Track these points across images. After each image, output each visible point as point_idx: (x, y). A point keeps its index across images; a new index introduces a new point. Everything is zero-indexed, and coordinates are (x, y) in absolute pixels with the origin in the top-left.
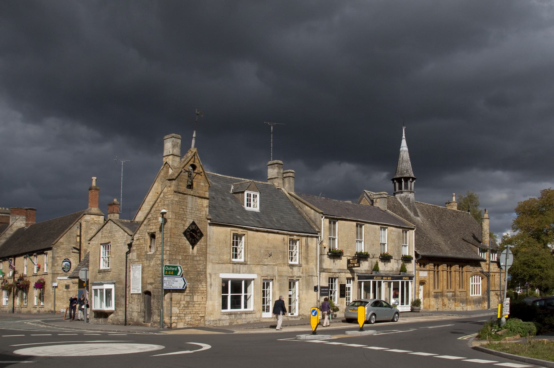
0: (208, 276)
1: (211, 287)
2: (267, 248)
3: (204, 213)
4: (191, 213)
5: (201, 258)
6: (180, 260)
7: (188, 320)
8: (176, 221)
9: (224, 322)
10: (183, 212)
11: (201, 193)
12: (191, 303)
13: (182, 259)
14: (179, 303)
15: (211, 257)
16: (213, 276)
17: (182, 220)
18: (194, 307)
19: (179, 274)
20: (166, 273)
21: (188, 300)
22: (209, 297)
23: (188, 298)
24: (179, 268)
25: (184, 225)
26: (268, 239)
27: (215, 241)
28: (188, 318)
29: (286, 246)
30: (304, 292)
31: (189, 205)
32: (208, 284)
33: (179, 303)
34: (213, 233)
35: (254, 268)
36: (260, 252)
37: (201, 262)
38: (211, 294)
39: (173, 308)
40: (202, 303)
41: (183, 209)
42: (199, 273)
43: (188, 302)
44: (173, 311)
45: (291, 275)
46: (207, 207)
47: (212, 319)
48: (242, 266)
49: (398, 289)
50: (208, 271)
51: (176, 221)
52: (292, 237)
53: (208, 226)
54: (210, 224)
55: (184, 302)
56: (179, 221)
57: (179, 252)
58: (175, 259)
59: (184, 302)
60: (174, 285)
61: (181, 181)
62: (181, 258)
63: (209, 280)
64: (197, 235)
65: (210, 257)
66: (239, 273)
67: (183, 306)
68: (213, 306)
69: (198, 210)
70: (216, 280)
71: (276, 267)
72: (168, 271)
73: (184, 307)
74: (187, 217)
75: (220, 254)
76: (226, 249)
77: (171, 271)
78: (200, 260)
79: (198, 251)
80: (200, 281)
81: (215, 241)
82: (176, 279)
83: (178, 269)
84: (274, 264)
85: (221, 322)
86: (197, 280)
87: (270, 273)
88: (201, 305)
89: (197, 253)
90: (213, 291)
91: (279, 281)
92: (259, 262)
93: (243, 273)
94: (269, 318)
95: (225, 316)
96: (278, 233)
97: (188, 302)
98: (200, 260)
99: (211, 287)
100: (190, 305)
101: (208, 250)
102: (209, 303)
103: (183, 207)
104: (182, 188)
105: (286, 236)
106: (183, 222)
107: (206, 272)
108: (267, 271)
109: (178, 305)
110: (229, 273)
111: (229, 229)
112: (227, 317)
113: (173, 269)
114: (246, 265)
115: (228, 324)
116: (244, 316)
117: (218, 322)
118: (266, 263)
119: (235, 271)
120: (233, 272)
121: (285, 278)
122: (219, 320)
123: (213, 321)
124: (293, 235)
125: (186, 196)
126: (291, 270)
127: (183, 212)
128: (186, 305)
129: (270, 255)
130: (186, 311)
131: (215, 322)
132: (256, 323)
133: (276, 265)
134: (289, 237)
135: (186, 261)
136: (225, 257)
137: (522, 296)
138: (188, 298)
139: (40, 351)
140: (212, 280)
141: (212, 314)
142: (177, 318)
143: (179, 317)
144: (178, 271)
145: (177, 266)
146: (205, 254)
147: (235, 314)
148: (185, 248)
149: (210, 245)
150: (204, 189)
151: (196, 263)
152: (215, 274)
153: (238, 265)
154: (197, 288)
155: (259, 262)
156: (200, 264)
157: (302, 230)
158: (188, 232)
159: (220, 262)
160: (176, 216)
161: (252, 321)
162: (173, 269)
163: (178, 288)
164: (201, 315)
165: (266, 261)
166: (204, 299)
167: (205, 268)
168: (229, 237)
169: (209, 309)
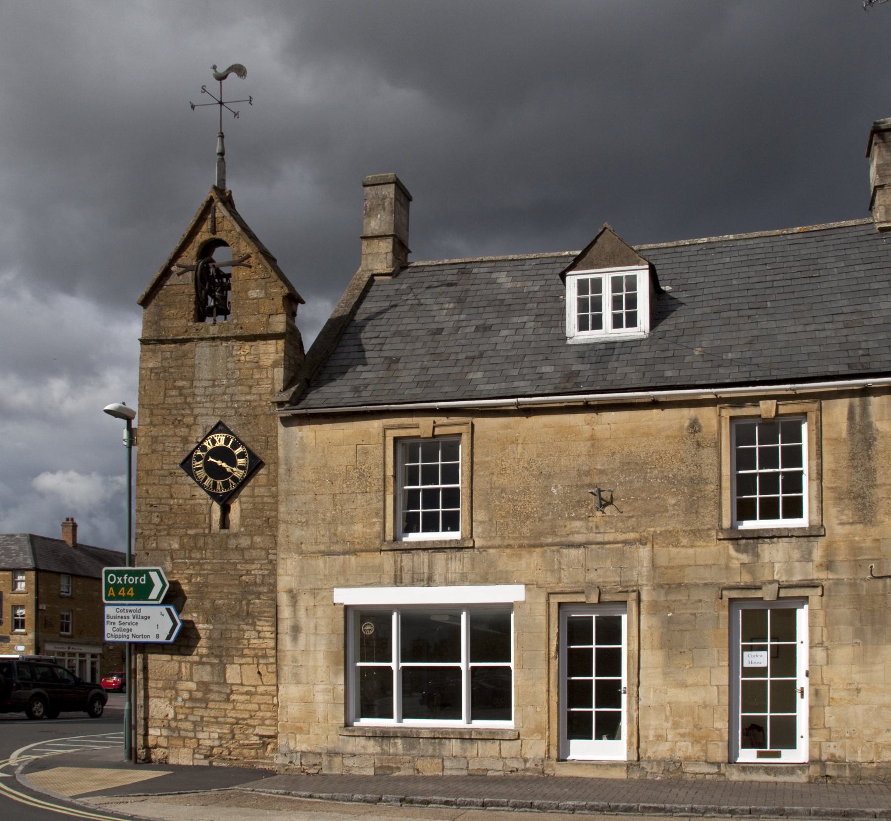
0: (283, 599)
1: (295, 639)
2: (580, 474)
3: (266, 387)
4: (211, 397)
5: (258, 539)
6: (172, 552)
7: (208, 743)
8: (155, 431)
9: (349, 762)
10: (179, 400)
11: (252, 323)
12: (214, 688)
13: (182, 547)
14: (172, 685)
15: (297, 533)
16: (305, 601)
17: (177, 423)
18: (228, 700)
19: (154, 594)
20: (112, 592)
21: (206, 678)
22: (286, 670)
23: (204, 674)
24: (154, 576)
25: (185, 440)
26: (593, 438)
27: (311, 476)
28: (209, 737)
29: (708, 454)
30: (843, 654)
31: (204, 373)
32: (285, 626)
33: (173, 688)
34: (303, 448)
35: (505, 561)
36: (546, 491)
37: (255, 553)
38: (295, 660)
39: (153, 702)
40: (261, 689)
41: (181, 388)
42: (247, 590)
43: (204, 686)
44: (153, 712)
45: (746, 579)
46: (275, 365)
47: (304, 747)
48: (440, 557)
49: (751, 646)
50: (285, 581)
51: (155, 431)
52: (748, 411)
53: (281, 429)
54: (287, 422)
55: (192, 686)
56: (168, 430)
57: (170, 527)
58: (157, 549)
59: (192, 686)
60: (136, 630)
61: (170, 305)
62: (176, 546)
63: (285, 612)
64: (233, 463)
65: (290, 533)
66: (429, 581)
67: (186, 695)
68: (306, 701)
69: (239, 382)
70: (320, 612)
71: (644, 552)
72: (117, 587)
73: (191, 699)
74: (197, 411)
75: (334, 521)
76: (360, 499)
77: (127, 586)
78: (252, 547)
79: (243, 517)
80: (250, 617)
81: (311, 476)
82: (145, 611)
83: (149, 579)
84: (632, 536)
85: (337, 760)
86: (238, 615)
87: (605, 573)
88: (257, 699)
89: (242, 525)
90: (306, 651)
91: (656, 608)
92: (541, 534)
93: (448, 583)
94: (614, 765)
95: (362, 741)
96: (655, 404)
97: (204, 686)
98: (252, 547)
99: (295, 639)
100: (212, 696)
101: (282, 508)
102: (290, 691)
103: (180, 383)
104: (176, 323)
105: (707, 415)
106: (183, 431)
107: (274, 585)
108: (582, 572)
109: (170, 693)
110: (380, 584)
111: (376, 425)
112: (372, 747)
113: (134, 580)
114: (467, 554)
115: (370, 772)
116: (454, 746)
117: (325, 760)
118: (579, 538)
119: (406, 577)
120: (398, 581)
121: (708, 596)
122: (332, 754)
123: (303, 754)
124: (755, 400)
125: (187, 346)
126: (745, 558)
127: (179, 400)
128: (199, 695)
129: (603, 504)
130: (201, 712)
131: (313, 760)
132: (523, 779)
133: (642, 542)
134: (728, 413)
135: (196, 555)
136: (358, 528)
137: (858, 542)
138: (204, 674)
139: (119, 778)
140: (302, 613)
141: (300, 730)
142: (165, 732)
143: (178, 729)
144: (150, 584)
145: (146, 572)
146: (271, 525)
147: (492, 736)
148: (193, 512)
149: (289, 493)
150: (267, 307)
151: (235, 557)
152: (314, 592)
153: (424, 556)
154: (239, 640)
155: (541, 534)
156: (252, 561)
157: (844, 370)
158: (199, 458)
159: (337, 548)
160: (152, 414)
161: (496, 769)
162: (134, 580)
163: (153, 639)
164: (260, 731)
165: (578, 529)
166: (270, 679)
167: (273, 573)
168: (379, 452)
169: (292, 711)
